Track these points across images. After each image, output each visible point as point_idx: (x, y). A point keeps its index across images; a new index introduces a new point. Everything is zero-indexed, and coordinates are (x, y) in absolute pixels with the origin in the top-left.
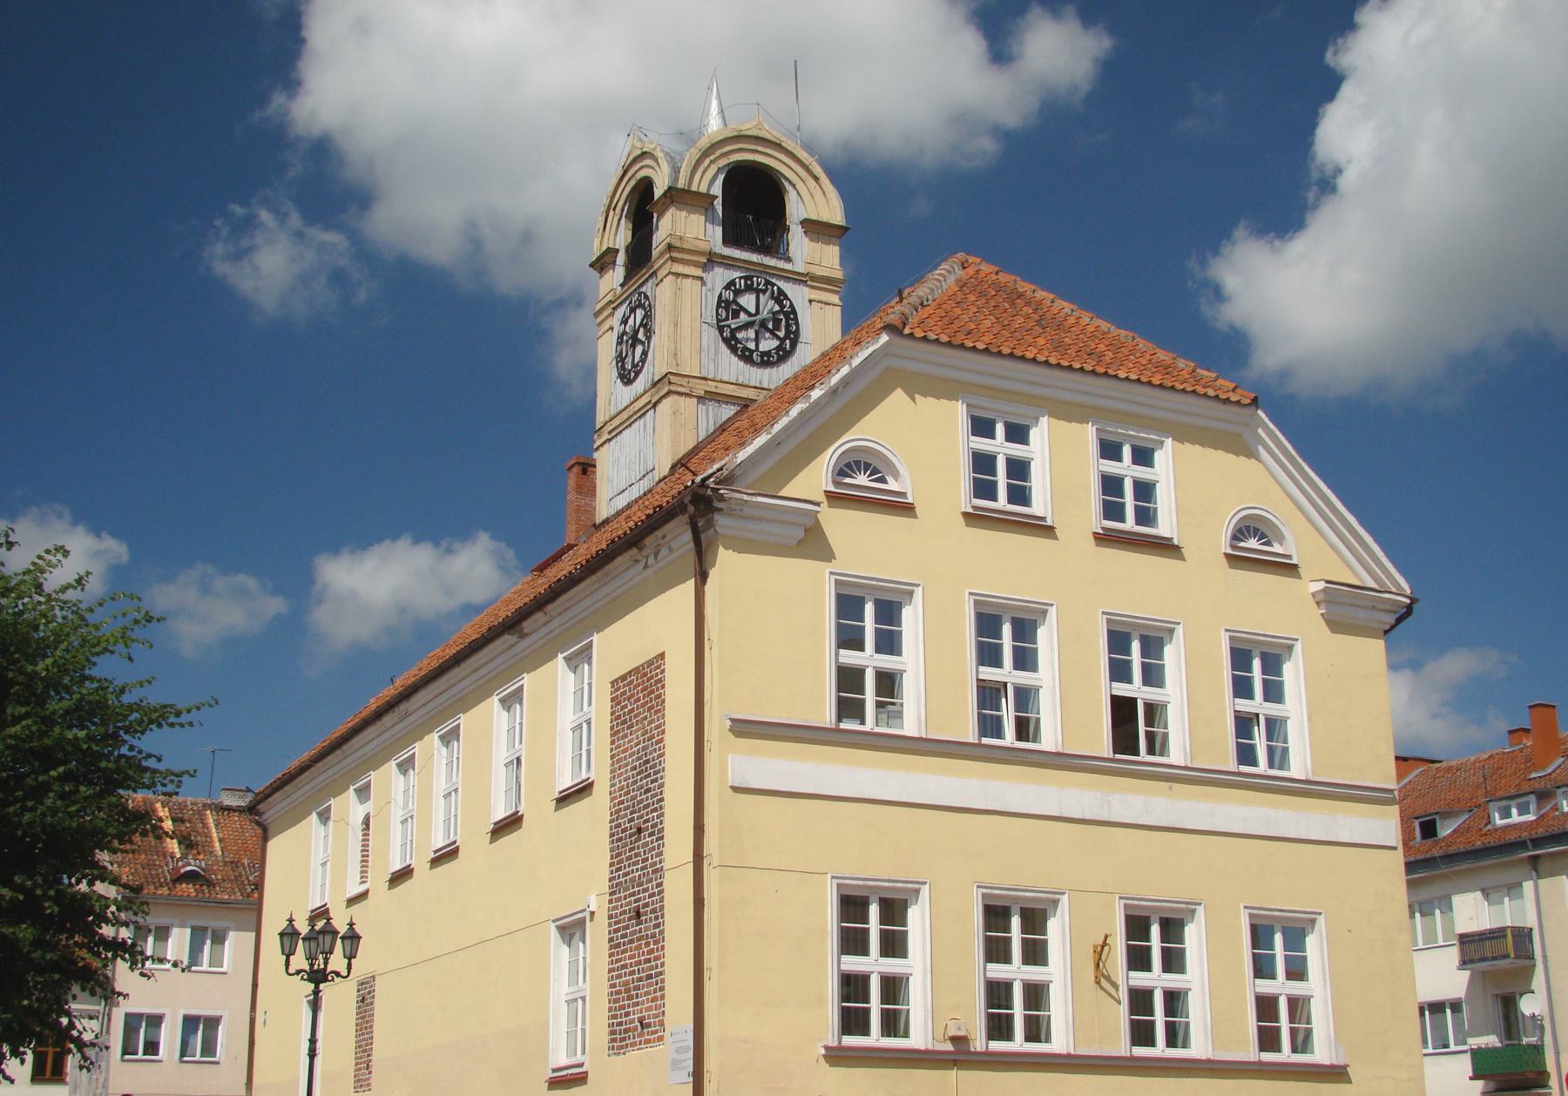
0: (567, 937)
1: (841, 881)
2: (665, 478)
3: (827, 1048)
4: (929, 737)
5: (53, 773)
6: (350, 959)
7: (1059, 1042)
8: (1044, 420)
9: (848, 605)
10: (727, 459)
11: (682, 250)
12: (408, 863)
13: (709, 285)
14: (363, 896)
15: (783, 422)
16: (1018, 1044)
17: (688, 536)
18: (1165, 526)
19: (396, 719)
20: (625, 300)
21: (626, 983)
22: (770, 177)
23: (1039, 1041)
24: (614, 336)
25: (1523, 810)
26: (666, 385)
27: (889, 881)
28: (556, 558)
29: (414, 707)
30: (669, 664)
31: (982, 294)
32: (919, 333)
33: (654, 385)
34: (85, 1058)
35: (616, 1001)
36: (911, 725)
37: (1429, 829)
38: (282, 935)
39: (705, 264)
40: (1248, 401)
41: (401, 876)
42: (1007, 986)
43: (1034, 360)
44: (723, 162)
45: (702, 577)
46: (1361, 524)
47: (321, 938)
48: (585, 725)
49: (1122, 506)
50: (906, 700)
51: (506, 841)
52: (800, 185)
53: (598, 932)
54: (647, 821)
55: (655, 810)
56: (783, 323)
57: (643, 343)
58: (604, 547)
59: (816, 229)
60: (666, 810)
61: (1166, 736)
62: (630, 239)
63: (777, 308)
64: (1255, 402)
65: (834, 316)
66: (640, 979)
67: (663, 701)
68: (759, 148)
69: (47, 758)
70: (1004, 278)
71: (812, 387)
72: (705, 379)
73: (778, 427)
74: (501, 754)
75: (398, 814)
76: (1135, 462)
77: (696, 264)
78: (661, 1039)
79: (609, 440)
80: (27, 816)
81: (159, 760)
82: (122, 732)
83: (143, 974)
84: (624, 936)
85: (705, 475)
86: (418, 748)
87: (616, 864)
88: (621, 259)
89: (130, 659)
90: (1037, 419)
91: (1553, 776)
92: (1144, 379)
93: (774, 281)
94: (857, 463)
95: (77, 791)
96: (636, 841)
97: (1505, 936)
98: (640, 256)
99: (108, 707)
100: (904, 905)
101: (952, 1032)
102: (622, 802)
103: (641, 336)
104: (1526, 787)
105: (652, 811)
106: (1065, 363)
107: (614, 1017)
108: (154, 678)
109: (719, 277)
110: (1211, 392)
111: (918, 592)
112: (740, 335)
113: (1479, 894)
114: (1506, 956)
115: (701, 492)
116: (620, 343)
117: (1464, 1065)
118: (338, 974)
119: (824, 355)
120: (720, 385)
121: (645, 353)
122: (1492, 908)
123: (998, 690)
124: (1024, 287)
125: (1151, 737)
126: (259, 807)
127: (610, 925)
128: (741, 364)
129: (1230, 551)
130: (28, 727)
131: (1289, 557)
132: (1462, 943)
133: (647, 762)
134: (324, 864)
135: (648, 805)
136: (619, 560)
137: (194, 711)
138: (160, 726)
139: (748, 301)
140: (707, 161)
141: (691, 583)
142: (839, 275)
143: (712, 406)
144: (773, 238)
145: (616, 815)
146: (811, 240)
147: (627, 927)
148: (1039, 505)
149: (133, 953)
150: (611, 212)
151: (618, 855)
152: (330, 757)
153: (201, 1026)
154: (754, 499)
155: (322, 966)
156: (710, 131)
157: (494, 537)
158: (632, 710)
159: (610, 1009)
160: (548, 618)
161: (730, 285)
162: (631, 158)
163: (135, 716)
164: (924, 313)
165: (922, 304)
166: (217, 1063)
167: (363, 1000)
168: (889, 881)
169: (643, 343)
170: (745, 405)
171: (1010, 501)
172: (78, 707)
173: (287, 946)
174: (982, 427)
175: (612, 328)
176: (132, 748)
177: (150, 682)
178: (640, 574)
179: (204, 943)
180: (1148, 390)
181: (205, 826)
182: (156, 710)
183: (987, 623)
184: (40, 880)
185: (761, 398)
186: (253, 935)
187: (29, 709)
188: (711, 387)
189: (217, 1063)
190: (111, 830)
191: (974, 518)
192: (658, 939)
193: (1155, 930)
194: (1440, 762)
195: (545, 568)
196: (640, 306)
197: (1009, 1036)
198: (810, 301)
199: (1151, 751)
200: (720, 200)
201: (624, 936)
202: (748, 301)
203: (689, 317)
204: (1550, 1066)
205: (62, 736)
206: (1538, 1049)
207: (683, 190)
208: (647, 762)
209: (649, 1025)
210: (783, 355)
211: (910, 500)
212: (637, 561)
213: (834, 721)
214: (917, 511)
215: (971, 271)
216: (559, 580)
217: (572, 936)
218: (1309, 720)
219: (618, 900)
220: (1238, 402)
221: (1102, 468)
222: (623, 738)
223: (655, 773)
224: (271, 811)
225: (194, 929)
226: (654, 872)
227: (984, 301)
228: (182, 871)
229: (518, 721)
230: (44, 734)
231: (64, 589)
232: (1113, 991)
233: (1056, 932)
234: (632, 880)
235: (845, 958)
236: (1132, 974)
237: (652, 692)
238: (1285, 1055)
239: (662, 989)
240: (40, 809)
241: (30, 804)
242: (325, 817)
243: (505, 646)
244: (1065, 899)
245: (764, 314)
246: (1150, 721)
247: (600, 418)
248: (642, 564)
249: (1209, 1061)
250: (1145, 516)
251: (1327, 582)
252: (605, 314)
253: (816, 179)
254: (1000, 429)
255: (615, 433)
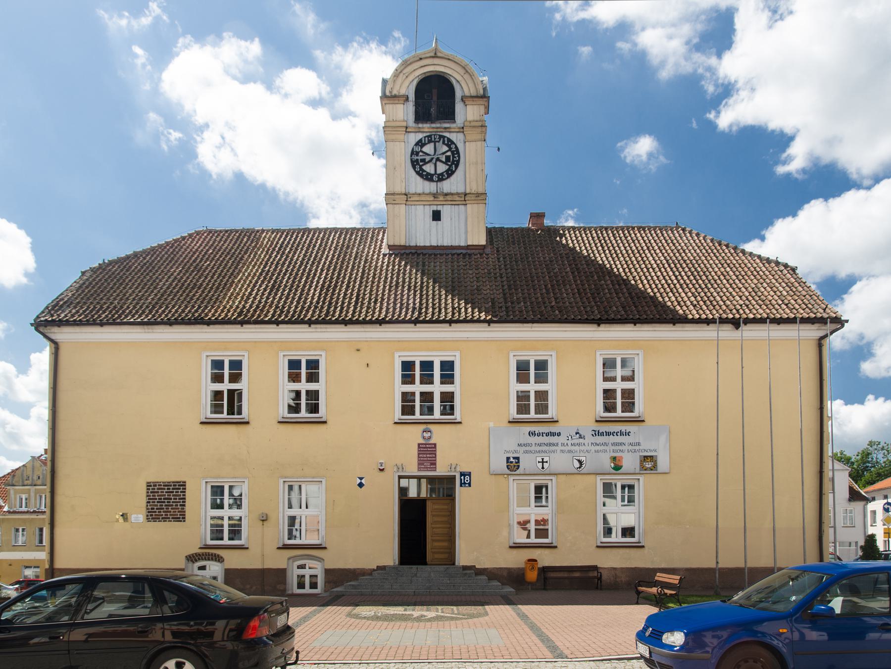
42: (614, 391)
44: (411, 78)
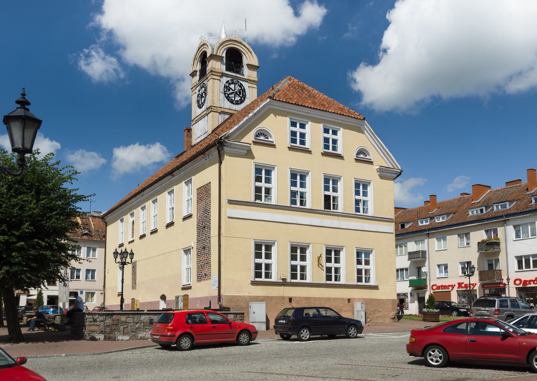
0: (186, 253)
1: (255, 241)
2: (210, 134)
3: (251, 281)
4: (278, 205)
5: (54, 213)
6: (131, 259)
7: (308, 280)
8: (310, 123)
9: (258, 170)
10: (227, 132)
11: (215, 72)
12: (144, 233)
13: (222, 82)
14: (133, 241)
15: (242, 122)
16: (298, 280)
17: (217, 152)
18: (339, 151)
19: (140, 196)
20: (199, 85)
21: (201, 265)
22: (238, 51)
23: (304, 280)
24: (196, 95)
25: (426, 222)
26: (210, 109)
27: (267, 241)
28: (182, 154)
29: (145, 193)
30: (212, 185)
31: (295, 88)
32: (278, 99)
33: (207, 109)
34: (65, 284)
35: (199, 269)
36: (273, 202)
37: (403, 226)
38: (114, 253)
39: (221, 76)
40: (362, 118)
41: (143, 236)
43: (307, 107)
44: (226, 47)
45: (221, 163)
46: (389, 151)
47: (124, 254)
48: (190, 200)
49: (329, 145)
50: (272, 195)
51: (170, 229)
52: (246, 54)
53: (194, 252)
54: (206, 225)
55: (208, 222)
56: (242, 93)
57: (204, 97)
58: (195, 154)
59: (251, 67)
60: (211, 222)
61: (337, 205)
62: (200, 68)
63: (240, 89)
64: (364, 119)
65: (255, 91)
66: (205, 264)
67: (210, 194)
68: (236, 44)
69: (52, 209)
70: (300, 83)
71: (249, 113)
72: (221, 108)
73: (240, 124)
74: (169, 206)
75: (141, 220)
76: (333, 134)
77: (218, 76)
78: (210, 278)
79: (195, 123)
80: (48, 224)
81: (81, 209)
82: (71, 202)
83: (79, 263)
84: (201, 253)
85: (221, 136)
86: (146, 204)
87: (198, 235)
88: (198, 73)
89: (72, 183)
90: (308, 122)
91: (434, 213)
92: (336, 112)
93: (239, 81)
94: (261, 133)
95: (60, 218)
96: (204, 230)
97: (420, 253)
98: (203, 73)
99: (67, 196)
100: (271, 246)
101: (282, 278)
102: (200, 220)
103: (204, 95)
104: (427, 216)
105: (208, 222)
106: (315, 108)
107: (198, 273)
108: (79, 189)
109: (225, 80)
110: (353, 116)
111: (276, 168)
112: (230, 96)
113: (414, 242)
114: (419, 258)
115: (220, 141)
116: (198, 97)
117: (408, 283)
118: (129, 263)
119: (252, 102)
120: (225, 109)
121: (205, 100)
122: (417, 246)
123: (296, 193)
124: (306, 86)
125: (334, 205)
126: (104, 218)
127: (197, 250)
128: (230, 104)
129: (356, 158)
130: (46, 201)
131: (371, 159)
132: (409, 254)
133: (206, 210)
134: (122, 233)
135: (207, 221)
136: (199, 157)
137: (89, 197)
138: (80, 201)
139: (232, 86)
140: (221, 47)
141: (218, 164)
142: (257, 80)
143: (223, 115)
144: (239, 68)
145: (198, 223)
146: (249, 70)
147: (201, 251)
148: (308, 145)
149: (74, 257)
150: (195, 60)
151: (199, 233)
152: (123, 206)
153: (91, 272)
154: (234, 143)
155: (124, 261)
156: (222, 38)
157: (161, 144)
158: (202, 197)
159: (197, 271)
160: (180, 172)
161: (227, 82)
162: (201, 45)
163: (74, 198)
164: (279, 93)
165: (279, 91)
166: (95, 281)
167: (134, 267)
168: (267, 241)
169: (204, 97)
170: (231, 115)
171: (300, 144)
172: (59, 196)
173: (115, 256)
174: (293, 124)
175: (196, 93)
176: (73, 206)
177: (77, 190)
178: (204, 161)
179: (90, 251)
180: (337, 115)
181: (89, 221)
182: (79, 197)
183: (294, 176)
184: (52, 240)
185: (236, 113)
186: (104, 249)
187: (46, 196)
188: (222, 110)
189: (95, 281)
190: (69, 227)
191: (291, 148)
192: (209, 254)
193: (333, 253)
194: (407, 209)
195: (179, 157)
196: (203, 87)
197: (296, 279)
198: (249, 87)
199: (334, 209)
200: (225, 58)
201: (201, 253)
202: (232, 86)
203: (216, 91)
204: (428, 284)
205: (55, 204)
206: (425, 280)
207: (215, 55)
208: (206, 210)
209: (207, 275)
210: (242, 101)
211: (274, 143)
212: (203, 158)
213: (254, 200)
214: (276, 146)
215: (292, 81)
216: (183, 162)
217: (187, 253)
218: (374, 201)
219: (199, 244)
220: (360, 119)
221: (324, 136)
222: (200, 203)
223: (209, 213)
224: (108, 219)
225: (88, 247)
226: (208, 238)
227: (295, 90)
228: (84, 233)
229: (173, 198)
230: (50, 203)
231: (53, 165)
232: (322, 268)
233: (308, 253)
234: (203, 239)
235: (256, 259)
236: (327, 264)
237: (208, 192)
238: (363, 283)
239: (210, 266)
240: (51, 222)
241: (48, 221)
242: (122, 221)
243: (169, 179)
244: (311, 245)
245: (237, 90)
246: (334, 201)
247: (193, 117)
248: (205, 159)
249: (345, 285)
250: (334, 148)
251: (380, 166)
252: (194, 89)
253: (251, 52)
254: (298, 125)
255: (197, 121)
